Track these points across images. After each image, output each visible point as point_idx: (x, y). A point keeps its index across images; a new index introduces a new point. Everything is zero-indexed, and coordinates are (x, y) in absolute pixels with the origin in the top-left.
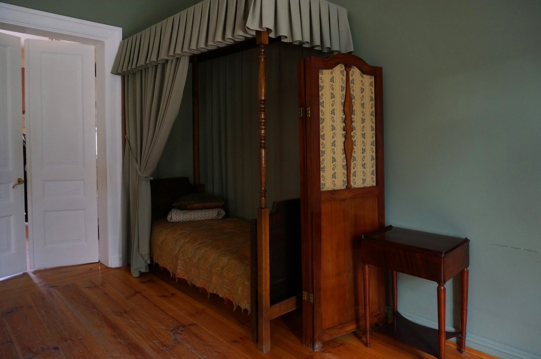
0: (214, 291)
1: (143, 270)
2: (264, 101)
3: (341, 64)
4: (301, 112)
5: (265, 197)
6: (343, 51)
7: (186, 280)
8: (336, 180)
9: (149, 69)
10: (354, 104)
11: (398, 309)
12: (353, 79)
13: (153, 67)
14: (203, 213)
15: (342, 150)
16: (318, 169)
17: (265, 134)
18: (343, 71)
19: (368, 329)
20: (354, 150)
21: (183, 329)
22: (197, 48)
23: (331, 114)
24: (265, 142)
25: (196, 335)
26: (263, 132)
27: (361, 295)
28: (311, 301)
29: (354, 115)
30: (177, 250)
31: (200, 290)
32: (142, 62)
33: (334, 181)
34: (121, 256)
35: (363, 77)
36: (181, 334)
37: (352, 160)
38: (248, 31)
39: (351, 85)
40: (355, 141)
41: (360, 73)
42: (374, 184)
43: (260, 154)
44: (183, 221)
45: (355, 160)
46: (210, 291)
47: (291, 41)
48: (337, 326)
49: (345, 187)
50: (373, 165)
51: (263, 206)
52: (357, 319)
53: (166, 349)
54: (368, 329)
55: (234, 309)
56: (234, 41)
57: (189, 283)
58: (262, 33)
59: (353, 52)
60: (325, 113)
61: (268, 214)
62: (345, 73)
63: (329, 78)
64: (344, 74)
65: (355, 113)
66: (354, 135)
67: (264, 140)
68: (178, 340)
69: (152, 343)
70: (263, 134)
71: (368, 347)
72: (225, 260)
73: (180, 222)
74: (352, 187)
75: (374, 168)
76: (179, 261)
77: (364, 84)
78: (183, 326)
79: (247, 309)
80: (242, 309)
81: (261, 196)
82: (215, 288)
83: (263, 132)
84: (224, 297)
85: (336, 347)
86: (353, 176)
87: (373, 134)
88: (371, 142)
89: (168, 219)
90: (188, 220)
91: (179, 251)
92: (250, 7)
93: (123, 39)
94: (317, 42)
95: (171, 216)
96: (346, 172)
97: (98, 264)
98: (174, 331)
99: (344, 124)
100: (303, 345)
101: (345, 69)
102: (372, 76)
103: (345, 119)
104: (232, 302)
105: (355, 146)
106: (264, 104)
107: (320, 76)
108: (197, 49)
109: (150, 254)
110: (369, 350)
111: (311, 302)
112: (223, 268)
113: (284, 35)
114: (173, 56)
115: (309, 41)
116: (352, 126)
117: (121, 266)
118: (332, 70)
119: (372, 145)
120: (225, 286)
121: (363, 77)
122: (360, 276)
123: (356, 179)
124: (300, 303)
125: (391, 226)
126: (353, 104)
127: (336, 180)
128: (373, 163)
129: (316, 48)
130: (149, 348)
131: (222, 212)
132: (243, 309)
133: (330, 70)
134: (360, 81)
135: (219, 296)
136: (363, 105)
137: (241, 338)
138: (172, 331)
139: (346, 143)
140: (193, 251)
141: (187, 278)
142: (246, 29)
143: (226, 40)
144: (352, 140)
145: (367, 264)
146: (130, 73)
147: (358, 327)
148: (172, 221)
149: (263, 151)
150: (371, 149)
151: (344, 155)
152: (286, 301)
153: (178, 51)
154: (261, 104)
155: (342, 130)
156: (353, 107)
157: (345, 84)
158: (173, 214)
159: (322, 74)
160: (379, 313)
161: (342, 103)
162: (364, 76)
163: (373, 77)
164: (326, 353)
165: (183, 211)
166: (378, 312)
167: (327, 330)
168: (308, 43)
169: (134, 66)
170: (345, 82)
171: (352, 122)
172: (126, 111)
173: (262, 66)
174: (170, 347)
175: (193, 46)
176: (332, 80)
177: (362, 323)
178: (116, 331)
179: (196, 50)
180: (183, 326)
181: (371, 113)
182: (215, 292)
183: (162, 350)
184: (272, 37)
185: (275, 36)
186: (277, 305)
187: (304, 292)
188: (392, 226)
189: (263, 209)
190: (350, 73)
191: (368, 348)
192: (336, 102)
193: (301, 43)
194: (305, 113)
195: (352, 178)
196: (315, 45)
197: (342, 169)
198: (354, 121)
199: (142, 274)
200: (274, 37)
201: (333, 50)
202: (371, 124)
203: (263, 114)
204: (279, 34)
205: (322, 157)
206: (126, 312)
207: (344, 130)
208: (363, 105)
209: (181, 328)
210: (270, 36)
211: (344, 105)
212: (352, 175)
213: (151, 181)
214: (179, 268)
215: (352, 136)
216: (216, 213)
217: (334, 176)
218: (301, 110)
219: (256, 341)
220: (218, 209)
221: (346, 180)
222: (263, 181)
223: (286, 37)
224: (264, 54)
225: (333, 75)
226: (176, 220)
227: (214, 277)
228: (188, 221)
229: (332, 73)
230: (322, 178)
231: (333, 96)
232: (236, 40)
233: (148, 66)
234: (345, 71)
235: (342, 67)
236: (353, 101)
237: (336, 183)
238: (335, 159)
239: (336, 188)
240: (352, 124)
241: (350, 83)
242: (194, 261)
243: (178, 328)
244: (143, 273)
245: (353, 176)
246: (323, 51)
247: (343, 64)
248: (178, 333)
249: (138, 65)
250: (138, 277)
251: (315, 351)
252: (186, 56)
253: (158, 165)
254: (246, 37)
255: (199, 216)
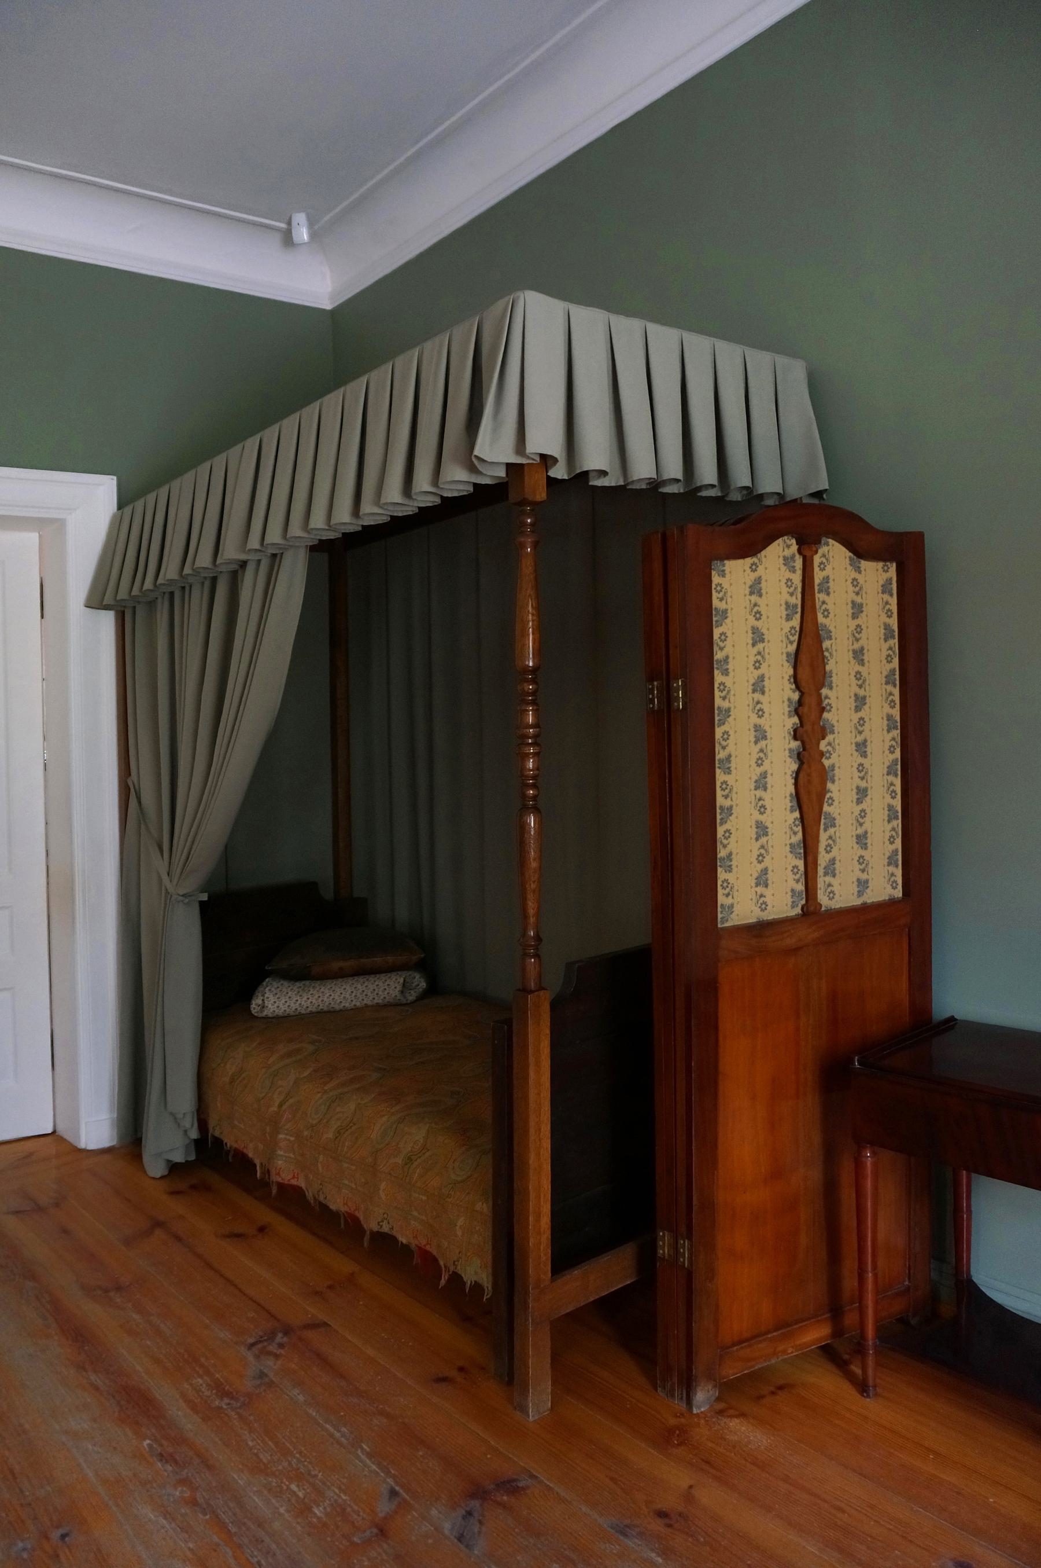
0: (381, 1226)
1: (178, 1157)
2: (535, 670)
3: (786, 537)
4: (653, 695)
5: (537, 956)
6: (794, 492)
7: (301, 1188)
8: (767, 892)
9: (192, 588)
10: (831, 654)
11: (973, 1272)
12: (826, 580)
13: (203, 584)
14: (359, 986)
15: (789, 798)
16: (710, 863)
17: (538, 769)
18: (793, 557)
19: (870, 1343)
20: (828, 796)
21: (285, 1339)
22: (330, 526)
23: (754, 691)
24: (536, 793)
25: (323, 1360)
26: (530, 764)
27: (848, 1218)
28: (684, 1260)
29: (831, 688)
30: (276, 1105)
31: (342, 1221)
32: (170, 571)
33: (761, 896)
34: (115, 1116)
35: (859, 567)
36: (277, 1356)
37: (822, 827)
38: (478, 467)
39: (820, 597)
40: (833, 766)
41: (851, 559)
42: (898, 893)
43: (523, 827)
44: (297, 1013)
45: (834, 826)
46: (371, 1225)
47: (621, 483)
48: (769, 1332)
49: (798, 910)
50: (891, 653)
51: (532, 985)
52: (835, 1310)
53: (229, 1404)
54: (870, 1343)
55: (443, 1282)
56: (442, 497)
57: (309, 1195)
58: (526, 468)
59: (826, 490)
60: (732, 692)
61: (546, 1008)
62: (799, 562)
63: (745, 583)
64: (794, 567)
65: (831, 682)
66: (830, 748)
67: (534, 786)
68: (266, 1375)
69: (191, 1385)
70: (531, 770)
71: (868, 1396)
72: (417, 1135)
73: (289, 1016)
74: (823, 909)
75: (898, 843)
76: (281, 1136)
77: (861, 588)
78: (287, 1331)
79: (480, 1282)
80: (464, 1284)
81: (525, 955)
82: (385, 1215)
83: (530, 764)
84: (414, 1243)
85: (763, 1397)
86: (826, 874)
87: (894, 739)
88: (887, 764)
89: (252, 1009)
90: (314, 1010)
91: (280, 1106)
92: (488, 391)
93: (121, 506)
94: (707, 472)
95: (263, 1000)
96: (801, 864)
97: (49, 1139)
98: (260, 1346)
99: (796, 720)
100: (657, 1391)
101: (799, 551)
102: (888, 563)
103: (800, 703)
104: (435, 1260)
105: (833, 782)
106: (534, 681)
107: (716, 579)
108: (330, 528)
109: (198, 1111)
110: (871, 1406)
111: (684, 1265)
112: (409, 1160)
113: (597, 468)
114: (260, 551)
115: (679, 474)
116: (821, 723)
117: (114, 1143)
118: (755, 560)
119: (887, 683)
120: (415, 1213)
121: (858, 570)
122: (846, 1178)
123: (835, 882)
124: (647, 1261)
125: (952, 1019)
126: (826, 654)
127: (767, 892)
128: (893, 829)
129: (704, 493)
130: (181, 1401)
131: (416, 979)
132: (469, 1283)
133: (749, 561)
134: (850, 581)
135: (398, 1241)
136: (859, 655)
137: (461, 1369)
138: (253, 1345)
139: (801, 775)
140: (323, 1107)
141: (303, 1185)
142: (472, 462)
143: (414, 497)
144: (823, 765)
145: (868, 1145)
146: (139, 602)
147: (838, 1332)
148: (265, 1013)
149: (532, 820)
150: (886, 788)
151: (797, 814)
152: (605, 1259)
153: (274, 536)
154: (525, 682)
155: (787, 738)
156: (824, 665)
157: (799, 596)
158: (266, 995)
159: (723, 574)
160: (908, 1288)
161: (788, 655)
162: (864, 564)
163: (894, 565)
164: (731, 1417)
165: (298, 984)
166: (907, 1283)
167: (733, 1345)
168: (677, 481)
169: (148, 584)
170: (800, 590)
171: (823, 710)
172: (130, 711)
173: (527, 567)
174: (242, 1399)
175: (318, 521)
176: (756, 588)
177: (850, 1319)
178: (86, 1348)
179: (327, 530)
180: (287, 1331)
181: (886, 677)
182: (385, 1228)
183: (219, 1408)
184: (560, 477)
185: (569, 473)
186: (576, 1272)
187: (661, 1234)
188: (956, 1020)
189: (531, 992)
190: (817, 559)
191: (868, 1400)
192: (769, 654)
193: (655, 485)
194: (668, 696)
195: (822, 881)
196: (698, 484)
197: (790, 856)
198: (828, 708)
199: (174, 1168)
200: (566, 477)
201: (761, 491)
202: (887, 709)
203: (532, 710)
204: (581, 467)
205: (721, 824)
206: (119, 1289)
207: (795, 738)
208: (859, 655)
209: (280, 1338)
210: (552, 476)
211: (796, 660)
212: (821, 871)
213: (202, 904)
214: (281, 1156)
215: (822, 754)
216: (397, 985)
217: (762, 880)
218: (653, 689)
219: (507, 1379)
220: (405, 974)
221: (804, 888)
222: (531, 912)
223: (603, 473)
224: (532, 531)
225: (761, 570)
226: (277, 1011)
227: (383, 1186)
228: (311, 1013)
229: (754, 568)
230: (723, 888)
231: (758, 637)
232: (445, 495)
233: (190, 581)
234: (797, 556)
235: (788, 546)
236: (826, 644)
237: (768, 899)
238: (767, 828)
239: (770, 915)
240: (821, 716)
241: (816, 591)
242: (325, 1136)
243: (271, 1336)
244: (177, 1163)
245: (826, 874)
246: (728, 499)
247: (793, 537)
248: (270, 1353)
249: (160, 581)
250: (162, 1177)
251: (695, 1411)
252: (298, 547)
253: (226, 847)
254: (475, 485)
255: (348, 996)
